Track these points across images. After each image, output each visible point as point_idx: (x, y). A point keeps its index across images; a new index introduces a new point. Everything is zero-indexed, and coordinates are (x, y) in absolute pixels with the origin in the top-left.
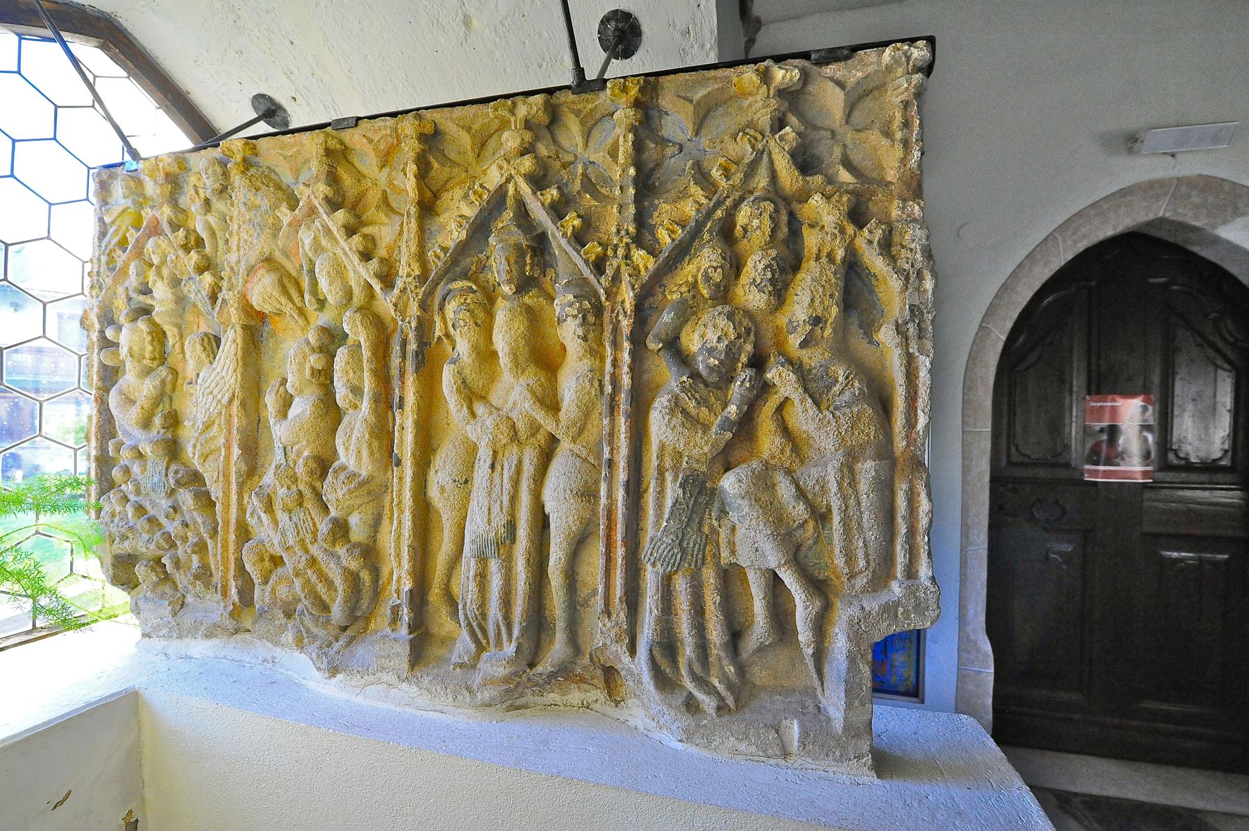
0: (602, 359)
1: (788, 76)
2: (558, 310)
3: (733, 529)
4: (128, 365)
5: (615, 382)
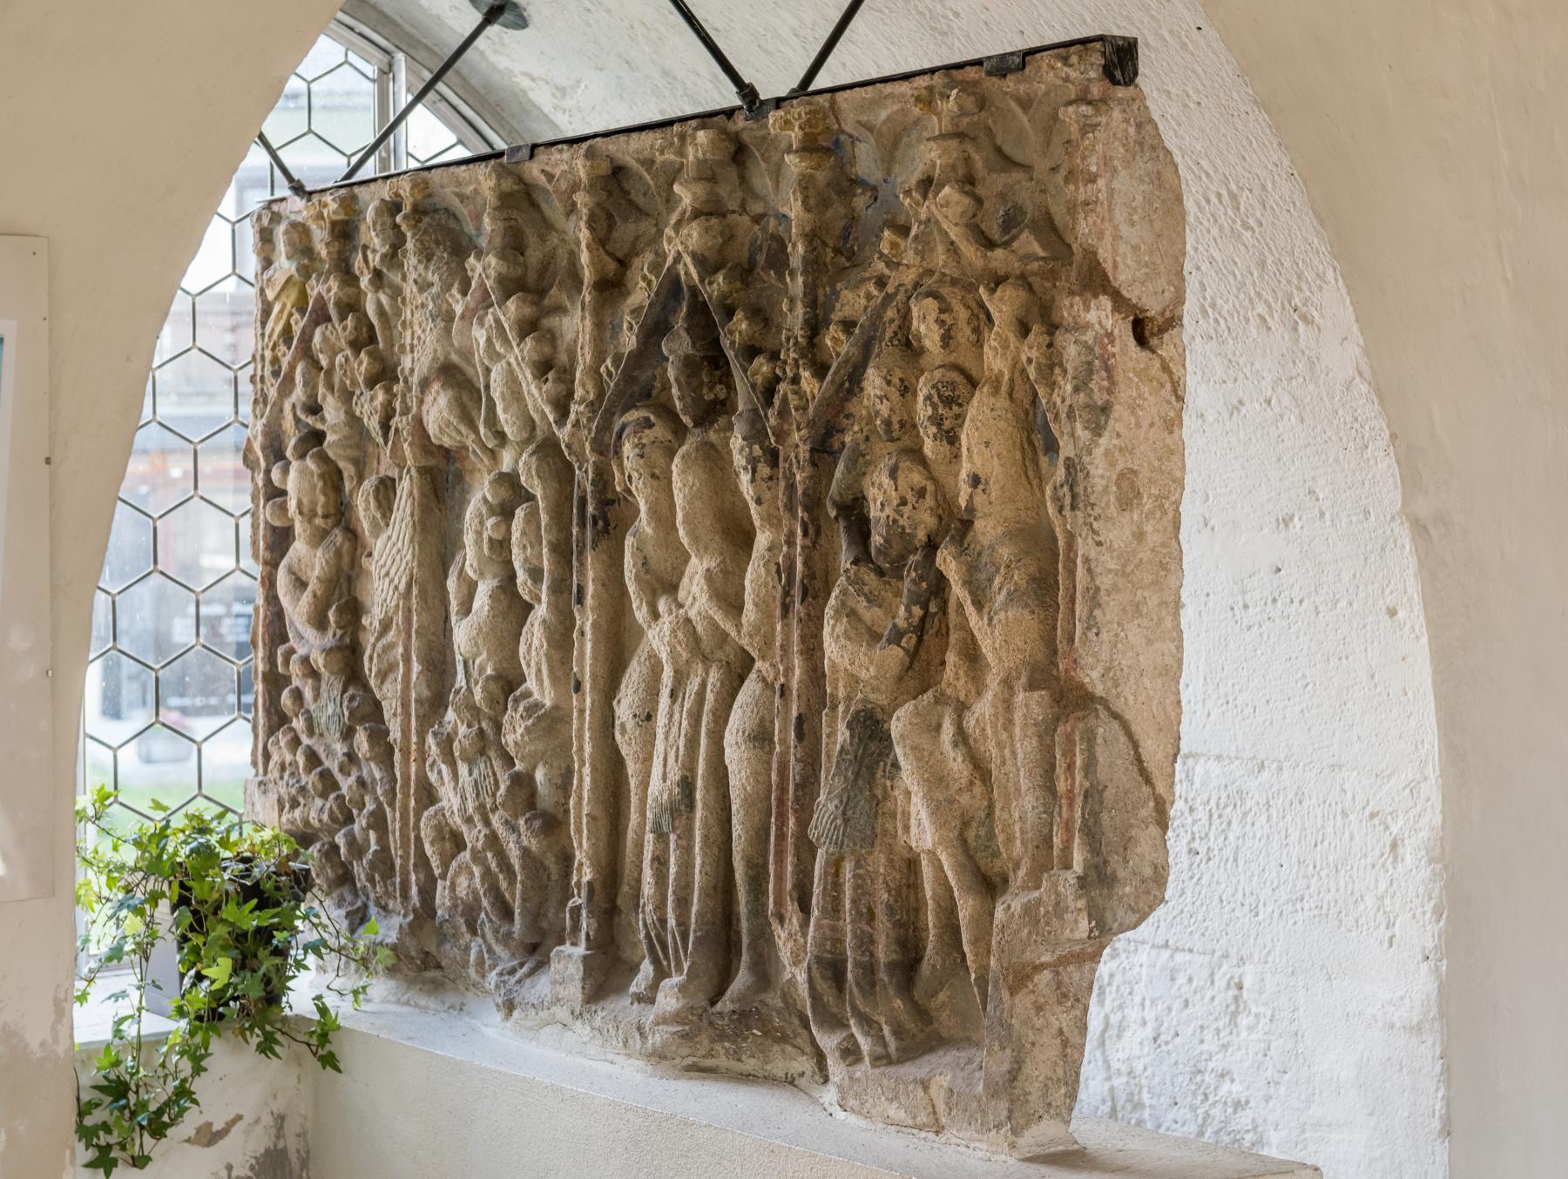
4: (298, 528)
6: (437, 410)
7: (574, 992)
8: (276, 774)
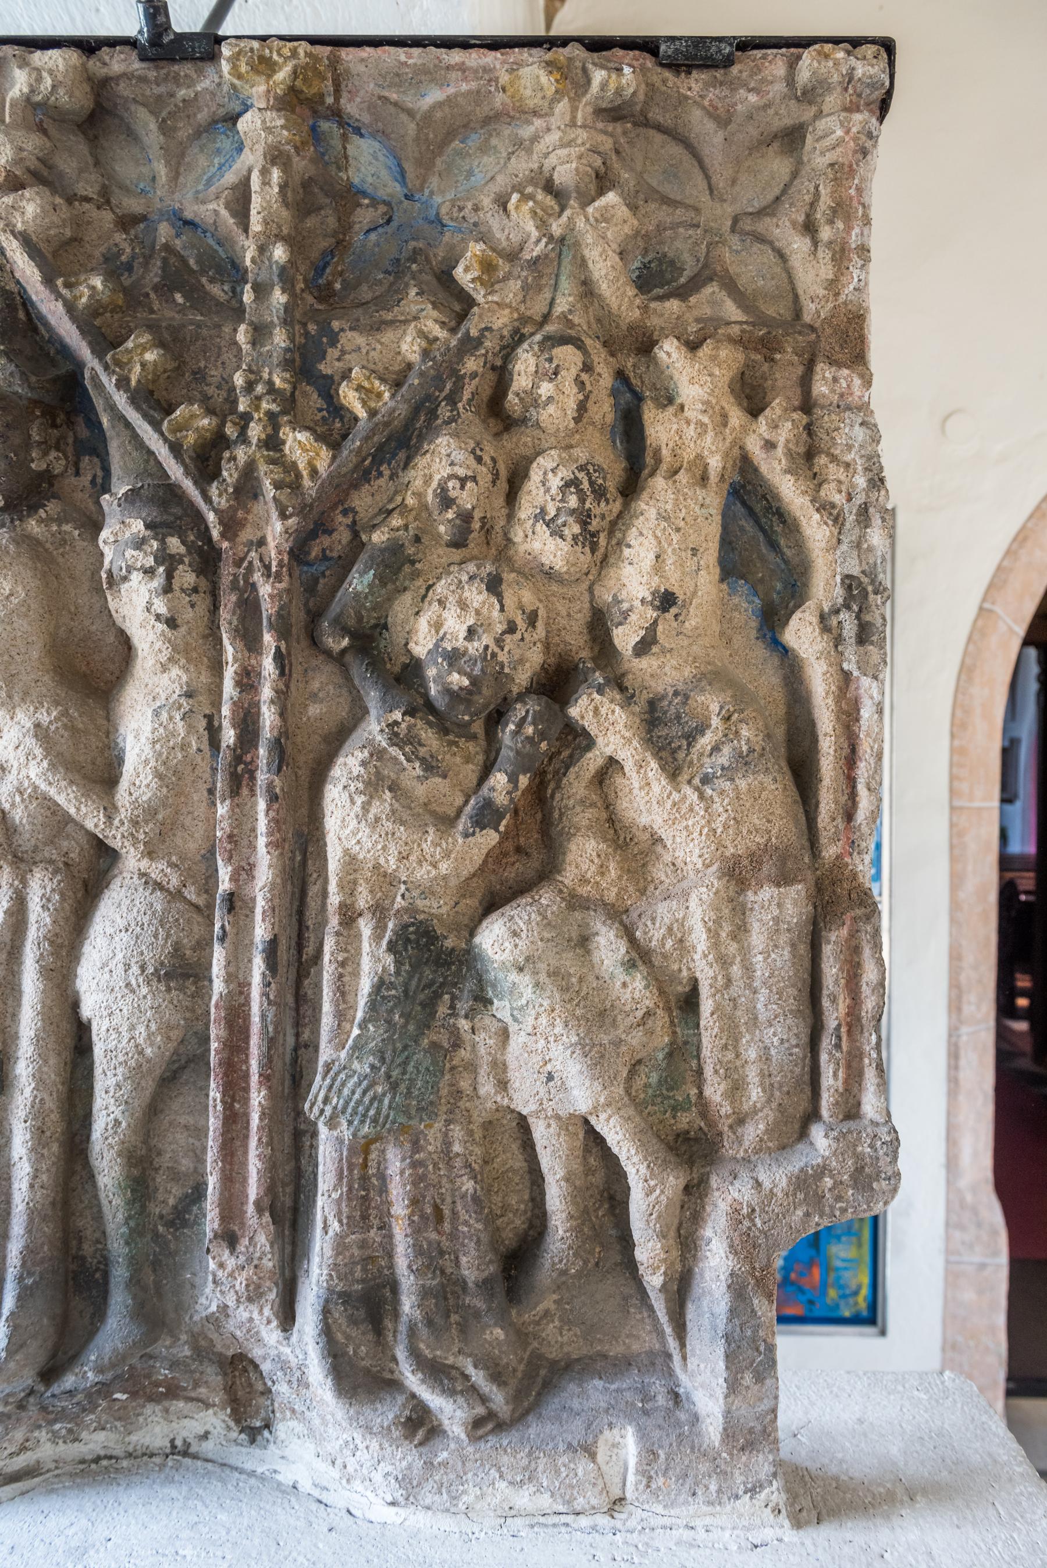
0: (217, 667)
1: (612, 86)
2: (109, 553)
3: (504, 1035)
5: (247, 723)
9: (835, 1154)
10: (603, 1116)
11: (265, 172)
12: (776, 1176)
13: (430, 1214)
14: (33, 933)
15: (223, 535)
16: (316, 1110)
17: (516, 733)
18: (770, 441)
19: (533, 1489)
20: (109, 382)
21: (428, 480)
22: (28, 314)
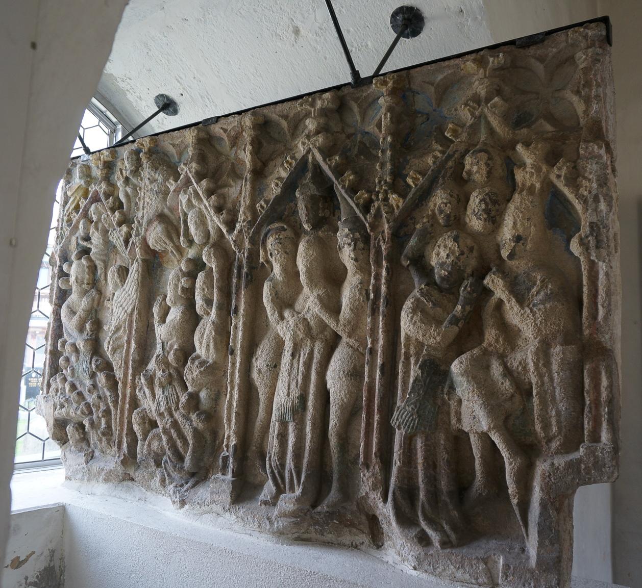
6: (155, 236)
7: (226, 498)
8: (54, 393)
9: (585, 455)
10: (493, 433)
11: (385, 115)
12: (560, 461)
13: (431, 464)
14: (315, 361)
15: (371, 231)
16: (394, 423)
17: (464, 290)
18: (558, 176)
19: (462, 571)
20: (340, 187)
21: (435, 205)
22: (320, 170)
